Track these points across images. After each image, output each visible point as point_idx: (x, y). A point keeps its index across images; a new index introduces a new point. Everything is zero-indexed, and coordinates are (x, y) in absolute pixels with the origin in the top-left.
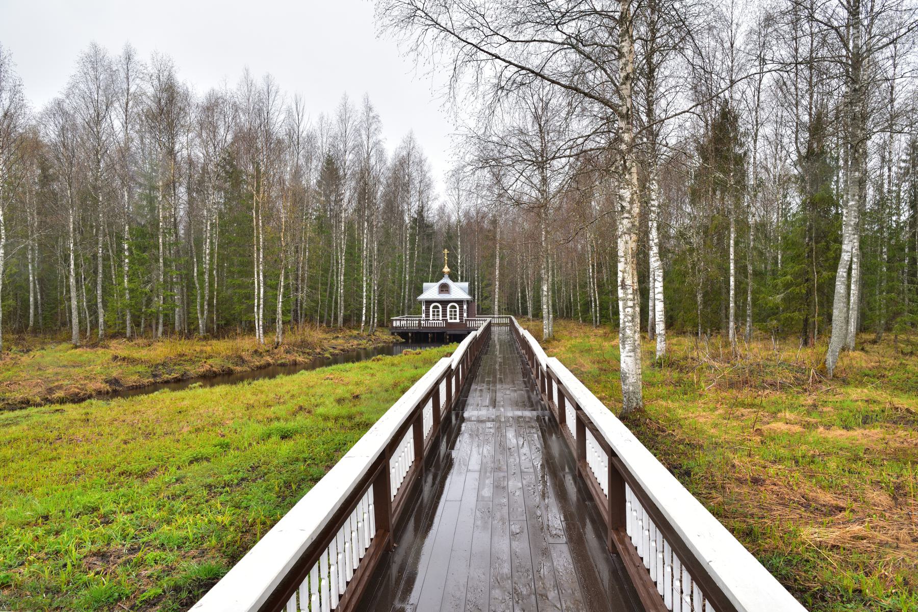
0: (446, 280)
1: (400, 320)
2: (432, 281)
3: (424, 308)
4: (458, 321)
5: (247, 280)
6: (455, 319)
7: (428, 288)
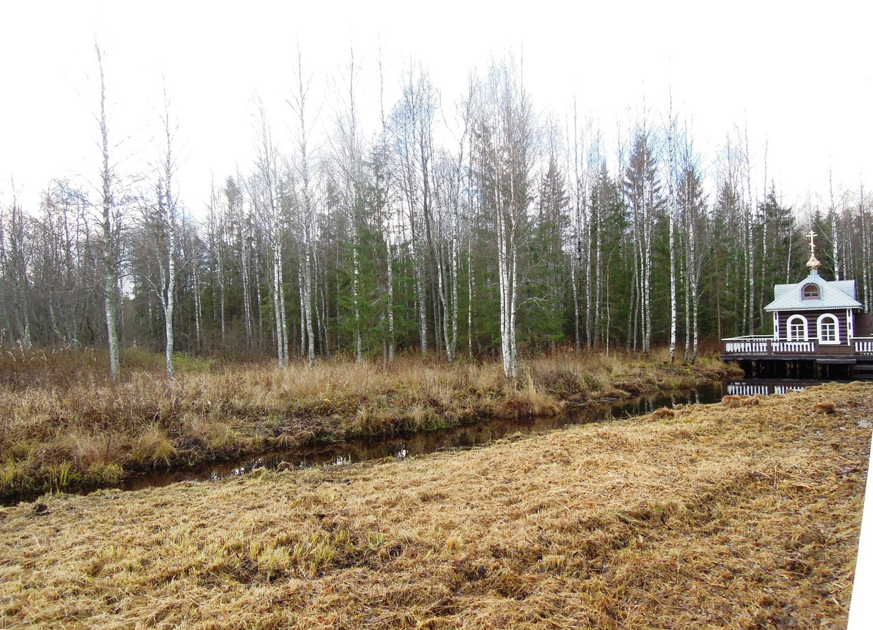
3: (776, 323)
4: (837, 342)
6: (832, 339)
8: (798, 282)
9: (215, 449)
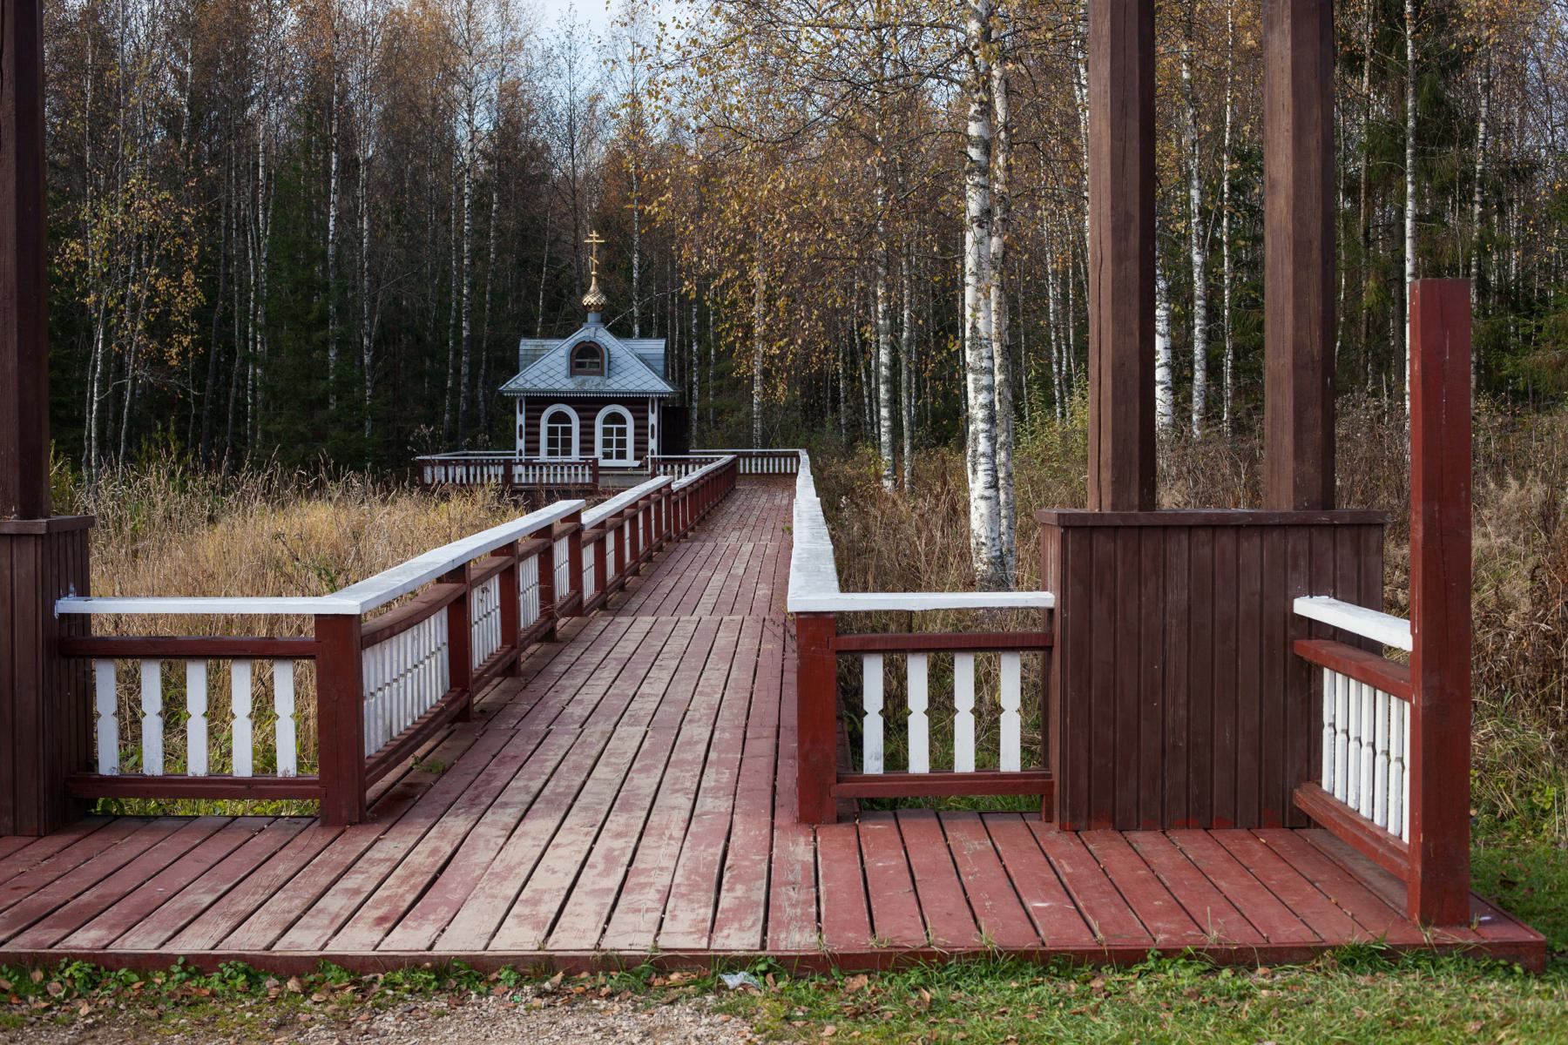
0: (593, 332)
1: (445, 463)
2: (548, 334)
3: (520, 419)
5: (655, 333)
6: (622, 455)
7: (535, 356)
8: (564, 337)
9: (319, 485)
